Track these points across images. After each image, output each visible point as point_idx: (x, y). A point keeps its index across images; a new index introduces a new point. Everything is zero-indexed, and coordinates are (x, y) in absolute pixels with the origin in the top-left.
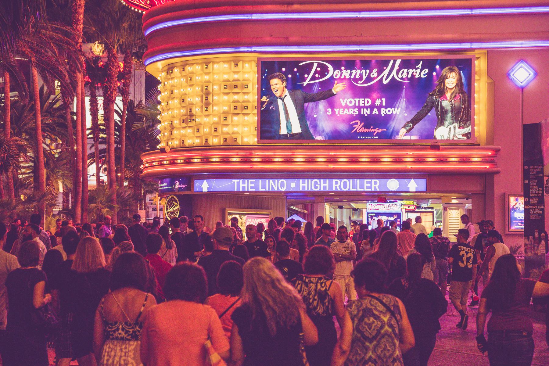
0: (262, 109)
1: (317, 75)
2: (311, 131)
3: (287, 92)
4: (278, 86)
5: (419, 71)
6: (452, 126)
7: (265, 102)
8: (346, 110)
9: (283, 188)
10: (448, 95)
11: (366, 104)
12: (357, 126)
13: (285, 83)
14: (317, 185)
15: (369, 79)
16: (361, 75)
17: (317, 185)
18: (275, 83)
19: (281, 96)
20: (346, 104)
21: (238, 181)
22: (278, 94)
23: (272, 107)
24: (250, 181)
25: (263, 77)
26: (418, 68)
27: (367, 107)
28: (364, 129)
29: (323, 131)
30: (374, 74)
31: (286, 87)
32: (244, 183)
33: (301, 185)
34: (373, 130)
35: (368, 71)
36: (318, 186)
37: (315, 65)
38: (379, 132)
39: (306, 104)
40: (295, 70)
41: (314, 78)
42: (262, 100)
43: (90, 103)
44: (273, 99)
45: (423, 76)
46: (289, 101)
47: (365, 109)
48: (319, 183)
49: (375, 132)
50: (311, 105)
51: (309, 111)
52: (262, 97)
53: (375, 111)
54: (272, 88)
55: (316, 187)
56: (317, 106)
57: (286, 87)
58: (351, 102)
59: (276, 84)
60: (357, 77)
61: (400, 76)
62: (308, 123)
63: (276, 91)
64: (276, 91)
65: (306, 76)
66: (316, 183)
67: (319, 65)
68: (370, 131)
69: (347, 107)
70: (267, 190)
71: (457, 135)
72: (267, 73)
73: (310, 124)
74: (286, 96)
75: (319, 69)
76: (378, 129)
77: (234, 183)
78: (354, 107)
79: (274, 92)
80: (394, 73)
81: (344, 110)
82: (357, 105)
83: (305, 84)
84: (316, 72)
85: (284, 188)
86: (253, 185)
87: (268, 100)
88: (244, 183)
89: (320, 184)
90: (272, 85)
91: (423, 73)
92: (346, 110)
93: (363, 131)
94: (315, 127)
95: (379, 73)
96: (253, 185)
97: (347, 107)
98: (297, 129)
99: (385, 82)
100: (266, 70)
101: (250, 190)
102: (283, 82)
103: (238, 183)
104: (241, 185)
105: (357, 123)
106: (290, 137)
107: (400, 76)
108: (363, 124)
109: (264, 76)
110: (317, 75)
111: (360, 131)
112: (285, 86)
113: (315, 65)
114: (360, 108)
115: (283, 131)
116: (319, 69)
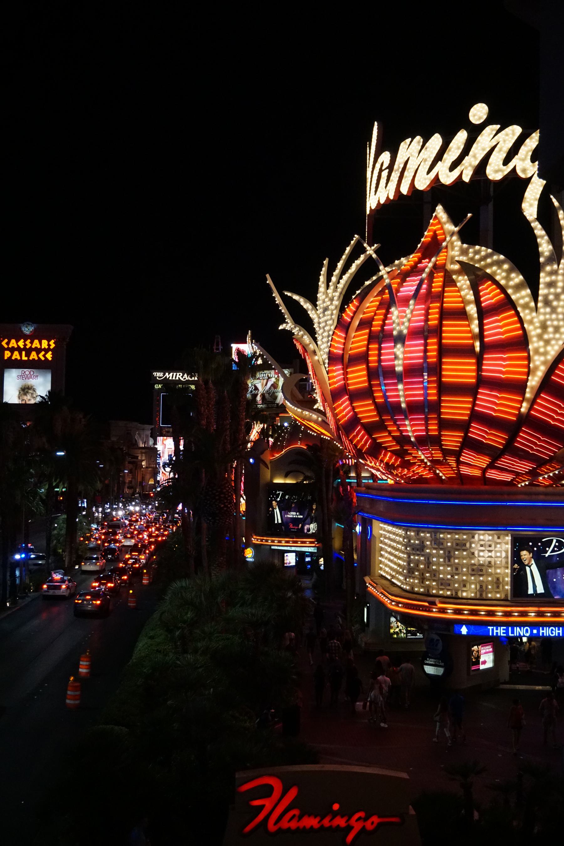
0: (514, 574)
1: (556, 549)
2: (552, 592)
3: (533, 562)
4: (526, 556)
7: (517, 568)
9: (527, 633)
12: (268, 803)
13: (531, 554)
14: (553, 632)
17: (553, 632)
18: (524, 554)
19: (528, 564)
21: (493, 627)
22: (526, 563)
23: (522, 572)
24: (502, 628)
25: (515, 549)
28: (300, 818)
29: (561, 592)
31: (532, 557)
32: (497, 629)
33: (541, 631)
34: (341, 822)
36: (554, 632)
37: (554, 541)
38: (369, 826)
39: (548, 571)
40: (539, 544)
41: (553, 551)
42: (514, 567)
44: (523, 566)
46: (534, 568)
48: (554, 630)
49: (349, 828)
50: (551, 571)
51: (550, 576)
52: (514, 565)
54: (522, 557)
55: (552, 633)
56: (556, 572)
57: (532, 557)
59: (525, 555)
62: (549, 586)
63: (525, 561)
64: (525, 561)
65: (547, 549)
66: (552, 630)
67: (557, 541)
68: (326, 822)
70: (515, 635)
72: (518, 546)
73: (551, 586)
74: (532, 564)
75: (557, 544)
76: (361, 814)
77: (489, 629)
79: (523, 561)
83: (547, 555)
84: (555, 546)
85: (528, 633)
86: (505, 631)
87: (519, 567)
88: (497, 629)
89: (555, 631)
90: (522, 556)
93: (293, 825)
94: (555, 588)
96: (505, 631)
98: (540, 589)
100: (531, 544)
101: (502, 635)
102: (530, 554)
103: (493, 630)
104: (495, 631)
105: (267, 791)
106: (536, 595)
108: (293, 793)
109: (516, 548)
110: (556, 549)
111: (285, 824)
112: (531, 556)
113: (554, 541)
115: (531, 591)
116: (557, 544)
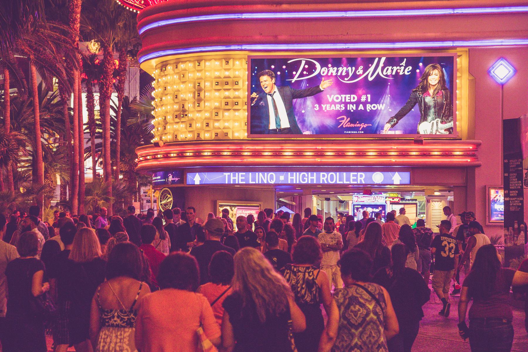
0: (252, 105)
1: (305, 73)
2: (300, 126)
3: (276, 89)
4: (267, 83)
5: (403, 68)
6: (435, 122)
7: (255, 98)
8: (333, 105)
9: (272, 180)
10: (431, 91)
11: (352, 100)
12: (343, 121)
13: (274, 79)
14: (305, 178)
15: (355, 76)
16: (347, 72)
17: (305, 178)
18: (265, 80)
19: (270, 92)
20: (333, 100)
21: (229, 174)
22: (267, 91)
23: (262, 103)
24: (240, 174)
25: (253, 74)
26: (402, 66)
27: (353, 103)
28: (350, 124)
29: (311, 126)
30: (360, 71)
31: (275, 84)
32: (234, 176)
33: (290, 178)
34: (359, 125)
35: (354, 68)
36: (306, 179)
37: (303, 62)
38: (365, 127)
39: (294, 100)
40: (284, 67)
41: (302, 75)
42: (252, 96)
43: (86, 99)
44: (263, 95)
45: (406, 73)
46: (278, 97)
47: (351, 105)
48: (306, 176)
49: (360, 127)
50: (299, 101)
51: (297, 106)
52: (252, 93)
53: (361, 107)
54: (262, 84)
55: (304, 180)
56: (305, 102)
57: (275, 84)
58: (337, 98)
59: (265, 81)
60: (344, 74)
61: (385, 73)
62: (297, 118)
63: (265, 88)
64: (265, 88)
65: (294, 73)
66: (304, 176)
67: (307, 63)
68: (356, 126)
69: (333, 103)
70: (257, 182)
71: (439, 130)
72: (257, 70)
73: (299, 119)
74: (275, 92)
75: (306, 66)
76: (363, 124)
77: (225, 176)
78: (341, 103)
79: (264, 89)
80: (379, 70)
81: (331, 106)
82: (343, 101)
83: (293, 81)
84: (304, 69)
85: (273, 181)
86: (244, 178)
87: (258, 96)
88: (234, 176)
89: (308, 177)
90: (262, 82)
91: (407, 70)
92: (333, 105)
93: (349, 126)
94: (303, 122)
95: (365, 70)
96: (244, 178)
97: (333, 103)
98: (285, 124)
99: (370, 79)
100: (256, 68)
101: (240, 182)
102: (272, 79)
103: (229, 176)
104: (232, 178)
105: (343, 119)
106: (279, 131)
107: (385, 73)
108: (349, 119)
109: (254, 73)
110: (305, 73)
111: (347, 126)
112: (274, 82)
113: (303, 62)
114: (346, 104)
115: (272, 126)
116: (306, 66)
